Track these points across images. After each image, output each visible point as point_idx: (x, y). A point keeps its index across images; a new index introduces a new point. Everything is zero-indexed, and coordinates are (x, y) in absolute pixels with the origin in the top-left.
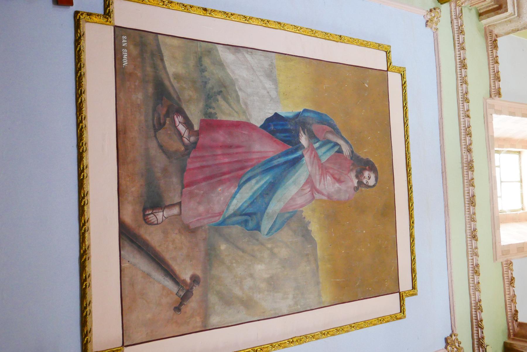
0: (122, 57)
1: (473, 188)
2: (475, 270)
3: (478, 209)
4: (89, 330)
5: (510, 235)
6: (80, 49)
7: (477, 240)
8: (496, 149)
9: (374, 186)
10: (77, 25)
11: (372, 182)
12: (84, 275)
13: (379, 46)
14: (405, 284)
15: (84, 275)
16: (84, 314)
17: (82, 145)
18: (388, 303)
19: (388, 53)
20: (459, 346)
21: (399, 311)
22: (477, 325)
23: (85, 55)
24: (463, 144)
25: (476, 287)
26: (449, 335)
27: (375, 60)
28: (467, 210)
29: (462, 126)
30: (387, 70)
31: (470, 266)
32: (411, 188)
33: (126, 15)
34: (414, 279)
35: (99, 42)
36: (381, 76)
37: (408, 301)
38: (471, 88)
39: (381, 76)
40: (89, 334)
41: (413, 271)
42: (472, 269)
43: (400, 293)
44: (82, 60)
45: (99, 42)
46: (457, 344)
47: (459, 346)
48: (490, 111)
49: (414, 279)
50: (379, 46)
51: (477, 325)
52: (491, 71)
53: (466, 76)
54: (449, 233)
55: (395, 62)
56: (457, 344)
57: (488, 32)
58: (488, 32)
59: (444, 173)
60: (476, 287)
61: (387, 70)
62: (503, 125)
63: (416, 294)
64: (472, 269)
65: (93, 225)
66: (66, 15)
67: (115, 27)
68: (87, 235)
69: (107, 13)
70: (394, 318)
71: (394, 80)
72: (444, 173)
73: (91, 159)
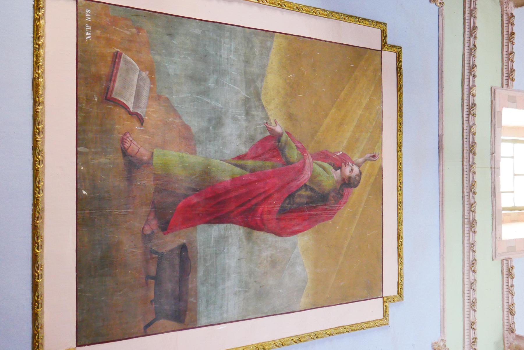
14: (389, 288)
18: (369, 310)
37: (392, 308)
55: (390, 41)
62: (510, 116)
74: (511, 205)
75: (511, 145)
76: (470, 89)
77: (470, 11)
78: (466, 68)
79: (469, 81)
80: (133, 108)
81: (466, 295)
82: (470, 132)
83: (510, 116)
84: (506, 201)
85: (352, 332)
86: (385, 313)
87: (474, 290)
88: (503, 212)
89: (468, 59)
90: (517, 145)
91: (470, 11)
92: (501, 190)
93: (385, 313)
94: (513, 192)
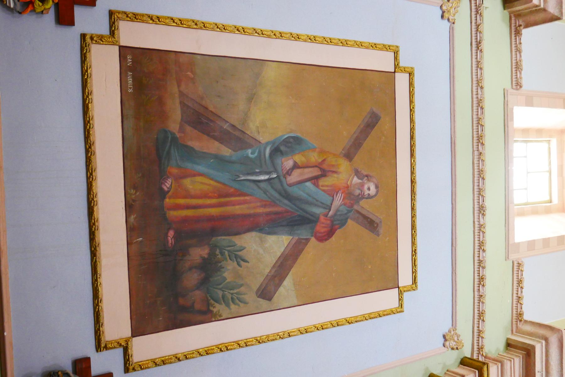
0: (127, 82)
5: (526, 230)
6: (96, 260)
9: (375, 195)
11: (373, 191)
13: (386, 48)
14: (405, 279)
17: (86, 46)
18: (386, 299)
19: (396, 53)
20: (458, 339)
23: (98, 212)
26: (447, 331)
27: (382, 62)
30: (395, 72)
32: (415, 250)
34: (414, 272)
36: (388, 78)
37: (406, 295)
39: (388, 78)
41: (413, 182)
43: (399, 288)
44: (98, 255)
45: (106, 66)
46: (456, 339)
47: (458, 339)
48: (510, 98)
49: (414, 272)
50: (386, 48)
54: (454, 121)
56: (456, 339)
57: (516, 264)
58: (516, 264)
59: (453, 144)
61: (395, 72)
62: (523, 116)
65: (103, 250)
67: (121, 47)
70: (392, 312)
71: (401, 80)
72: (453, 144)
73: (100, 186)
74: (524, 201)
75: (524, 145)
76: (478, 62)
77: (477, 10)
78: (474, 43)
79: (477, 55)
80: (179, 132)
81: (476, 165)
82: (477, 30)
83: (523, 116)
84: (518, 198)
85: (370, 320)
86: (404, 70)
87: (482, 126)
88: (515, 207)
89: (478, 201)
90: (529, 144)
91: (477, 10)
92: (514, 188)
93: (404, 70)
94: (526, 189)
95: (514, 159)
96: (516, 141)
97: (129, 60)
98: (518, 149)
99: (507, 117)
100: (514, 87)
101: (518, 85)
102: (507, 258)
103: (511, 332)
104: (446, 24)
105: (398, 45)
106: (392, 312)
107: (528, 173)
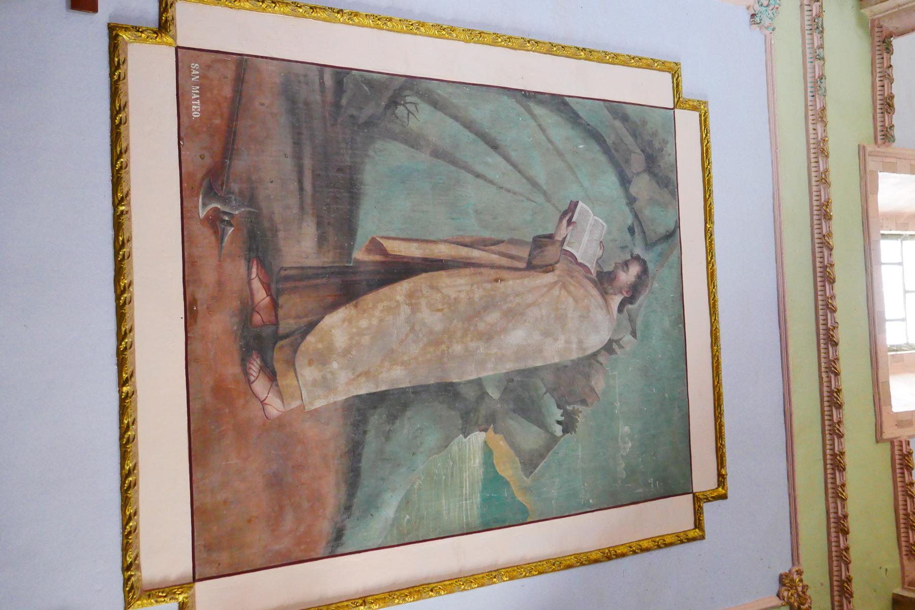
0: (189, 108)
1: (822, 62)
2: (835, 463)
3: (837, 225)
4: (122, 59)
7: (827, 156)
8: (882, 232)
10: (114, 46)
12: (116, 59)
14: (703, 478)
15: (116, 59)
16: (120, 257)
20: (803, 593)
21: (693, 527)
22: (839, 556)
24: (813, 169)
25: (836, 493)
28: (815, 198)
29: (835, 578)
31: (807, 18)
33: (199, 27)
35: (152, 72)
37: (708, 508)
38: (831, 70)
40: (127, 245)
42: (821, 270)
45: (152, 72)
46: (800, 589)
48: (871, 165)
51: (839, 556)
52: (879, 124)
53: (839, 422)
55: (687, 91)
60: (836, 493)
62: (895, 191)
63: (724, 497)
64: (821, 270)
65: (144, 431)
66: (91, 29)
67: (177, 48)
68: (121, 85)
69: (164, 26)
70: (684, 539)
77: (842, 589)
90: (906, 243)
91: (842, 589)
95: (887, 324)
96: (884, 236)
97: (195, 96)
98: (887, 250)
99: (867, 190)
100: (879, 141)
101: (886, 135)
102: (879, 438)
103: (873, 141)
104: (756, 35)
105: (706, 537)
106: (684, 539)
107: (906, 292)
